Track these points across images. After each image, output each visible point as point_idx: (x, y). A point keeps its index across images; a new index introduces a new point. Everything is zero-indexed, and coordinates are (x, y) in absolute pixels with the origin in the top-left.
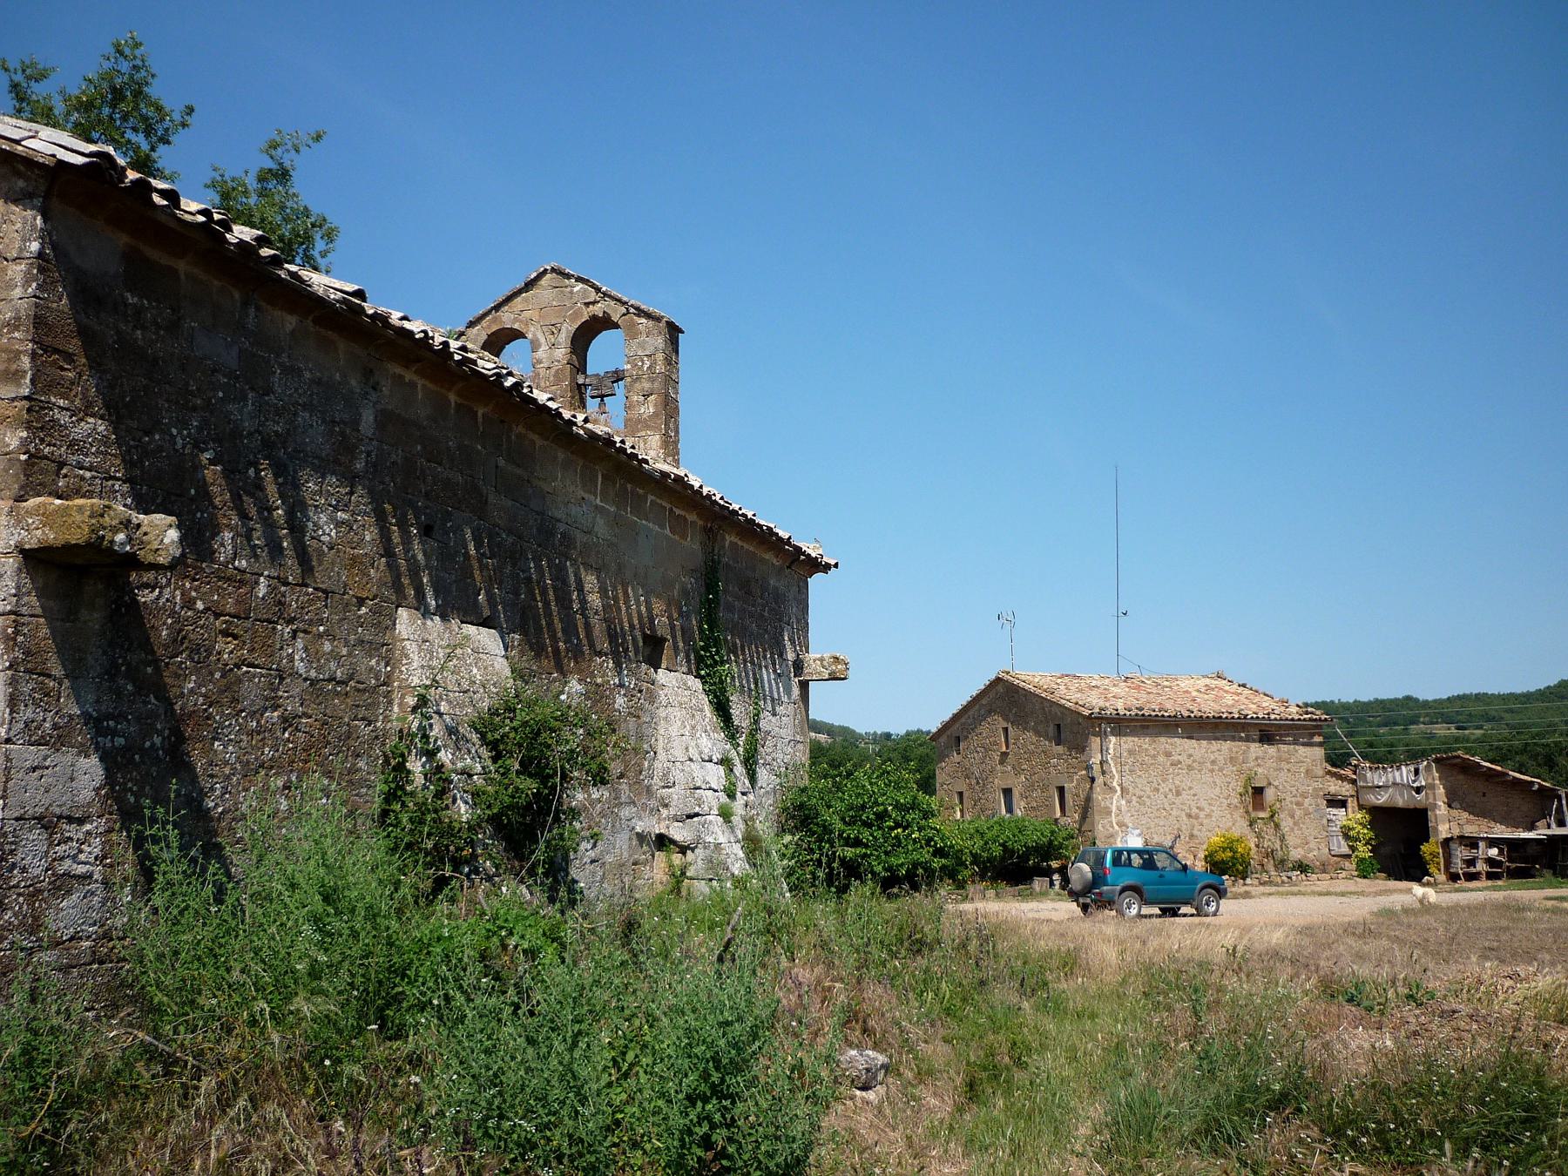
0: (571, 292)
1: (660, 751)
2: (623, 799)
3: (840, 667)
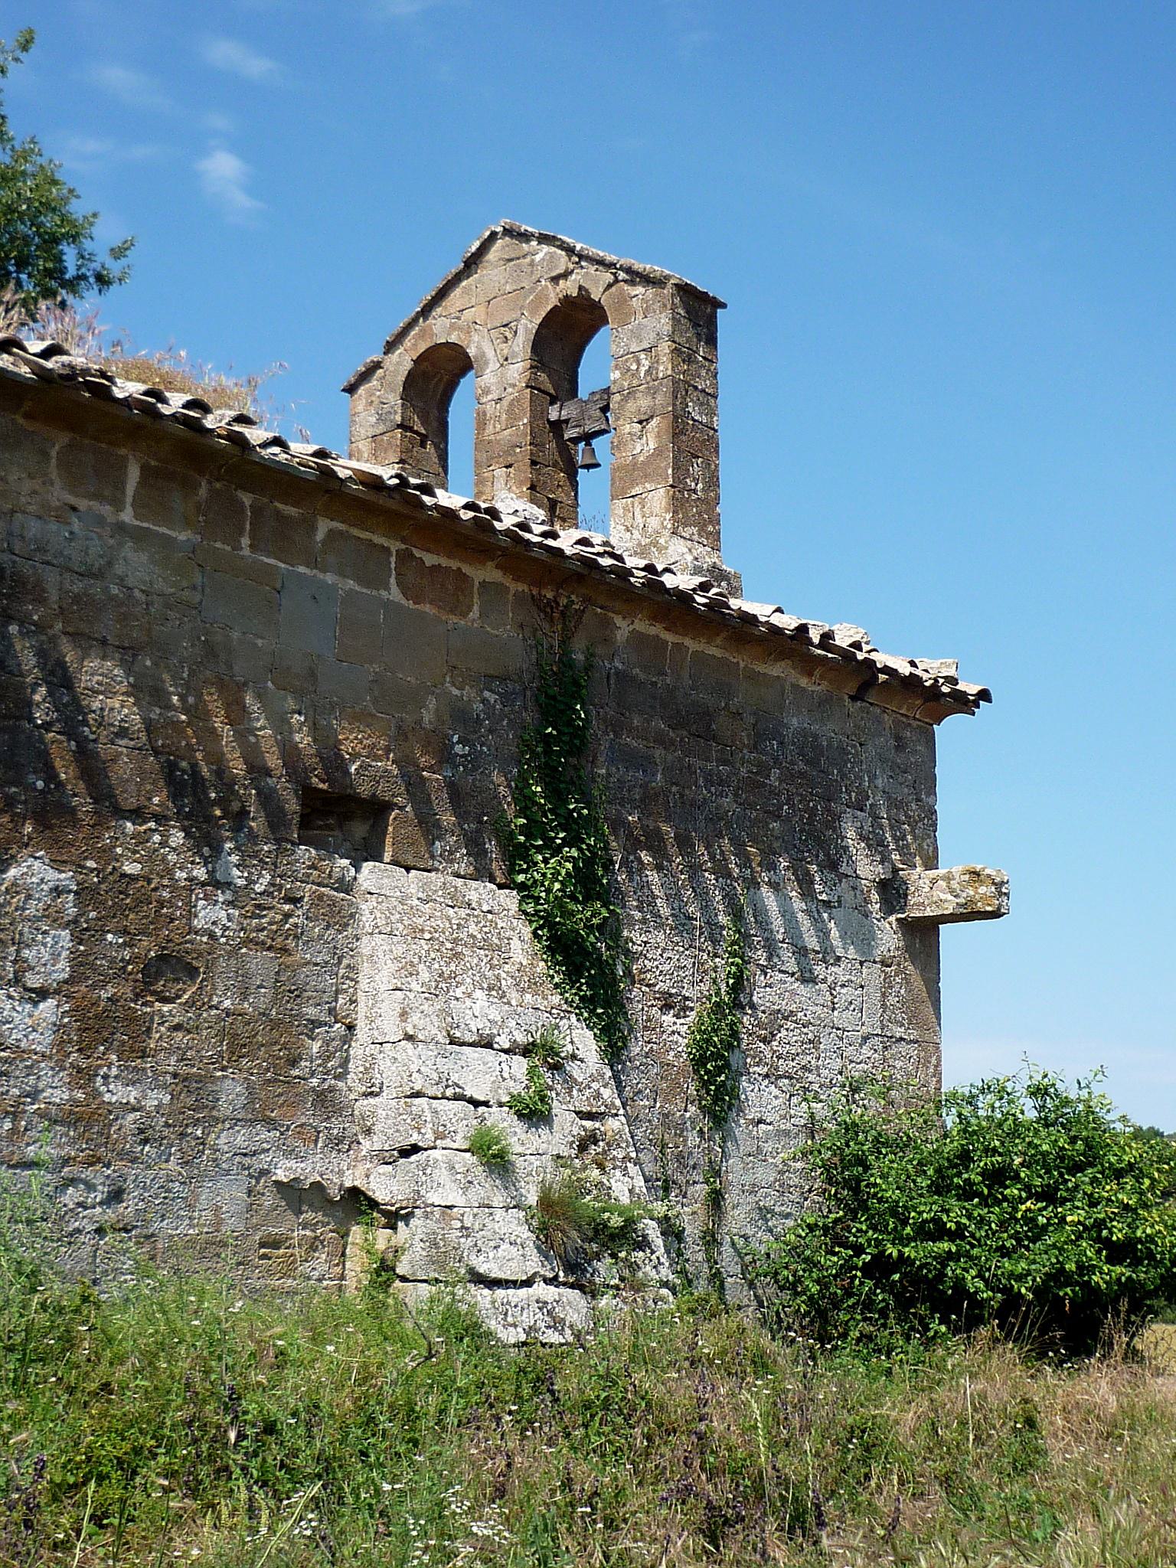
0: (532, 264)
1: (361, 1024)
2: (224, 1108)
3: (982, 890)
